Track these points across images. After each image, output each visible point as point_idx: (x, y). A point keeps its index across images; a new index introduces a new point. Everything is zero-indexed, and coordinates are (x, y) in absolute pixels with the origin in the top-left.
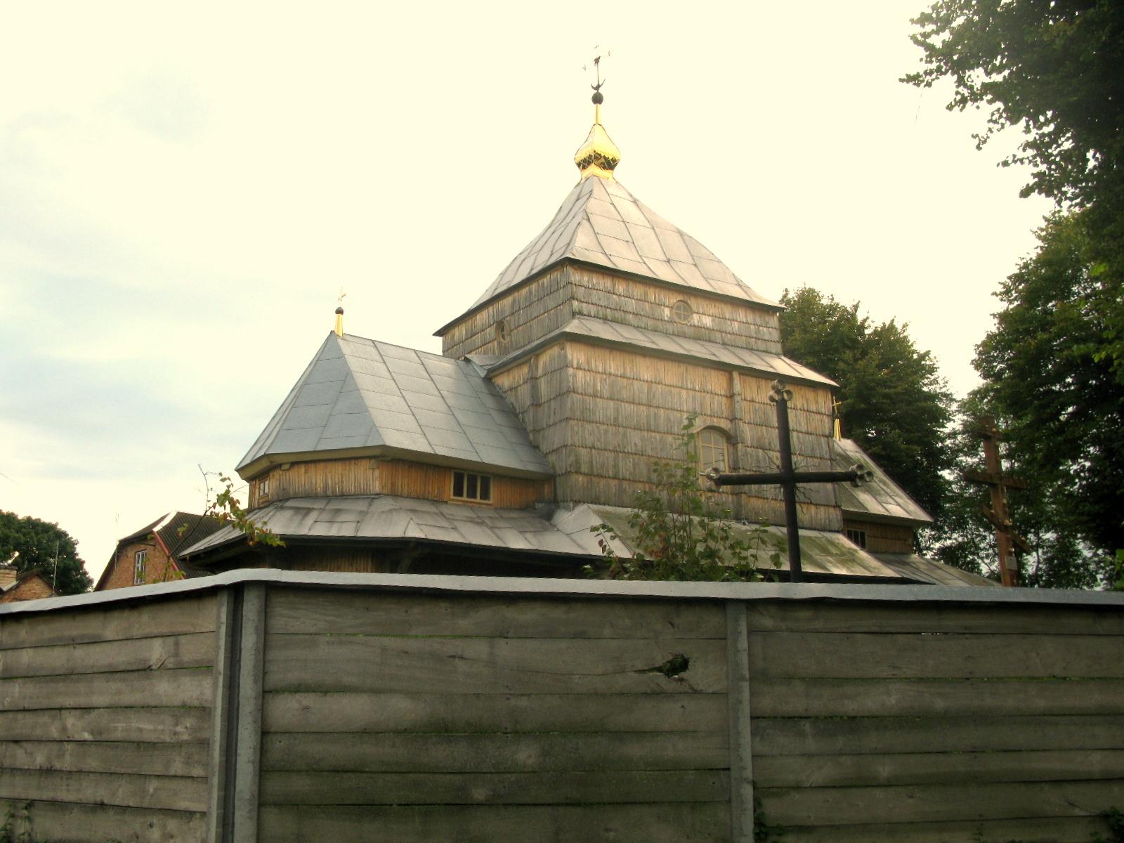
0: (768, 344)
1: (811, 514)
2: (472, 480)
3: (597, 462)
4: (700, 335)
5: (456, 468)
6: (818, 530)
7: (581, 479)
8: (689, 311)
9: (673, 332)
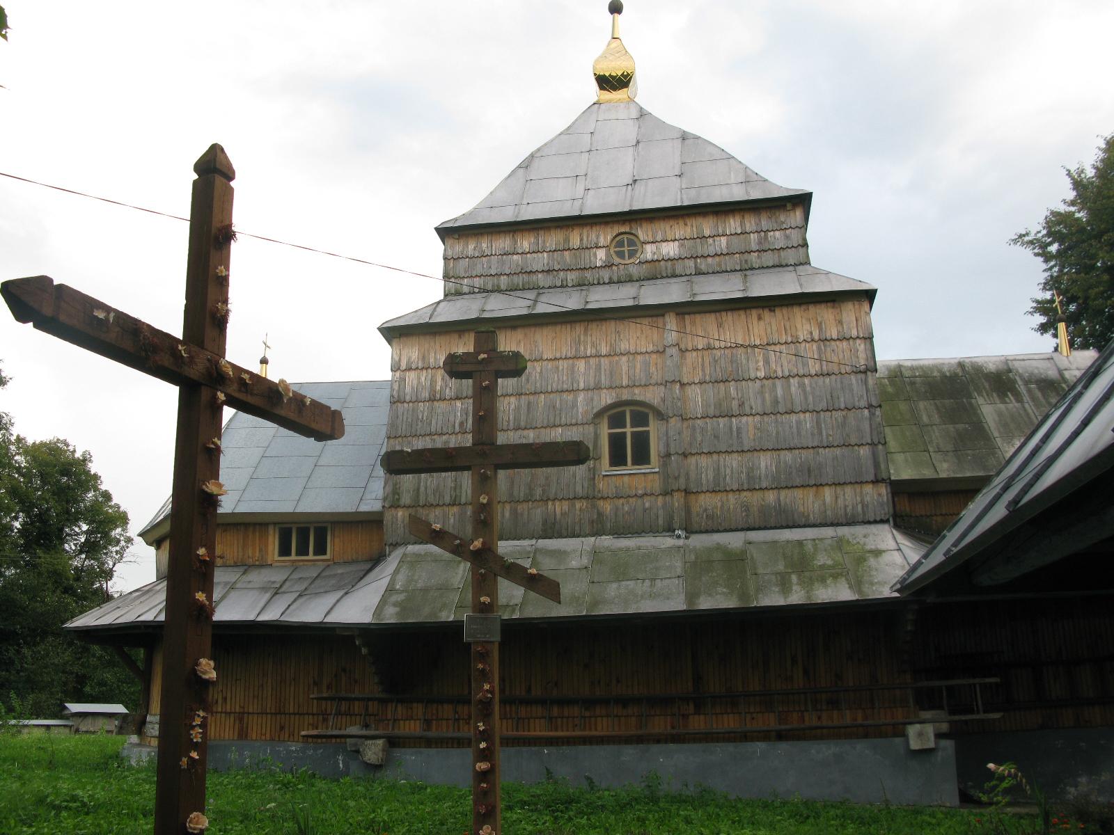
0: (782, 253)
1: (824, 501)
2: (303, 534)
3: (426, 488)
4: (657, 272)
5: (279, 523)
6: (832, 525)
7: (400, 514)
8: (634, 246)
9: (610, 278)
